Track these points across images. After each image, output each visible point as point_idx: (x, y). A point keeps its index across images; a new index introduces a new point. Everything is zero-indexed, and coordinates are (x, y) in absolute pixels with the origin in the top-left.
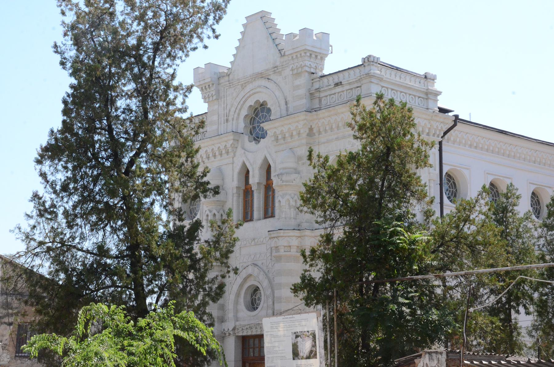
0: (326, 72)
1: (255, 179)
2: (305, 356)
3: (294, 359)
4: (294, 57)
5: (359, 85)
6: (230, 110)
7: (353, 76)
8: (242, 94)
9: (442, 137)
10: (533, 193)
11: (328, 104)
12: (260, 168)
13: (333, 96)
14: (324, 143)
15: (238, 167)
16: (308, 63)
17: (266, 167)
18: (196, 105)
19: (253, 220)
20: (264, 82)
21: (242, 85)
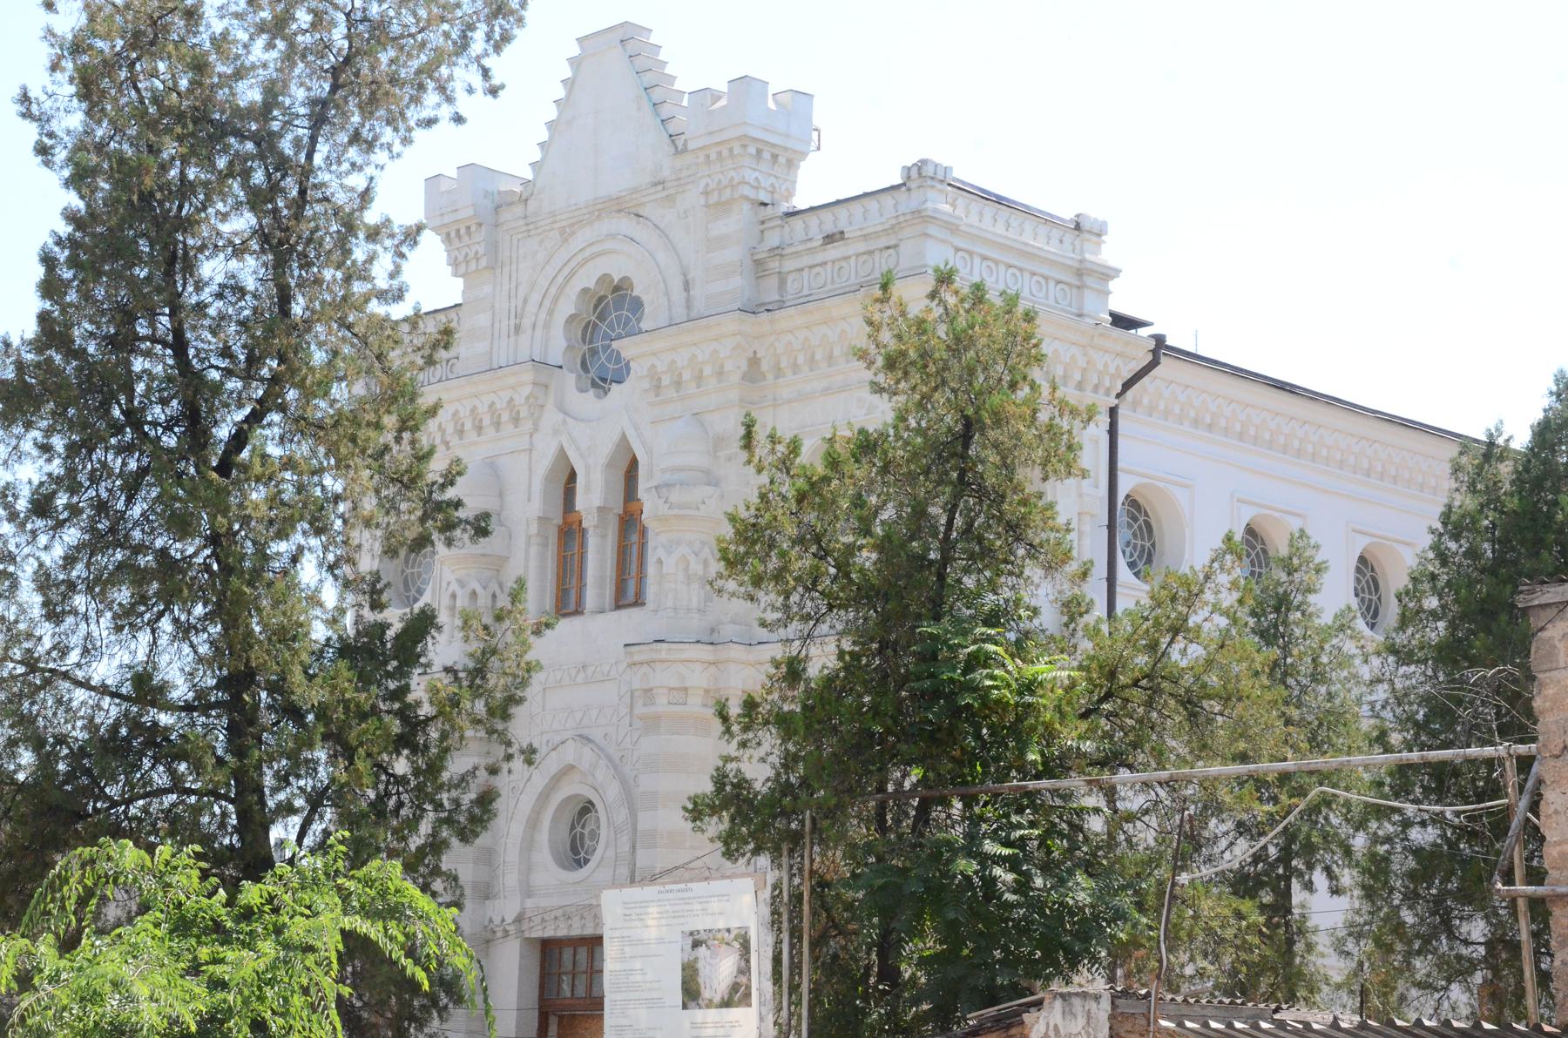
0: (801, 201)
1: (593, 496)
2: (717, 999)
4: (713, 157)
5: (892, 243)
6: (525, 301)
7: (878, 216)
9: (1118, 396)
10: (1362, 560)
11: (806, 292)
12: (610, 465)
13: (891, 251)
14: (789, 401)
15: (544, 461)
16: (750, 175)
17: (625, 465)
18: (430, 281)
19: (581, 613)
20: (625, 225)
21: (562, 231)
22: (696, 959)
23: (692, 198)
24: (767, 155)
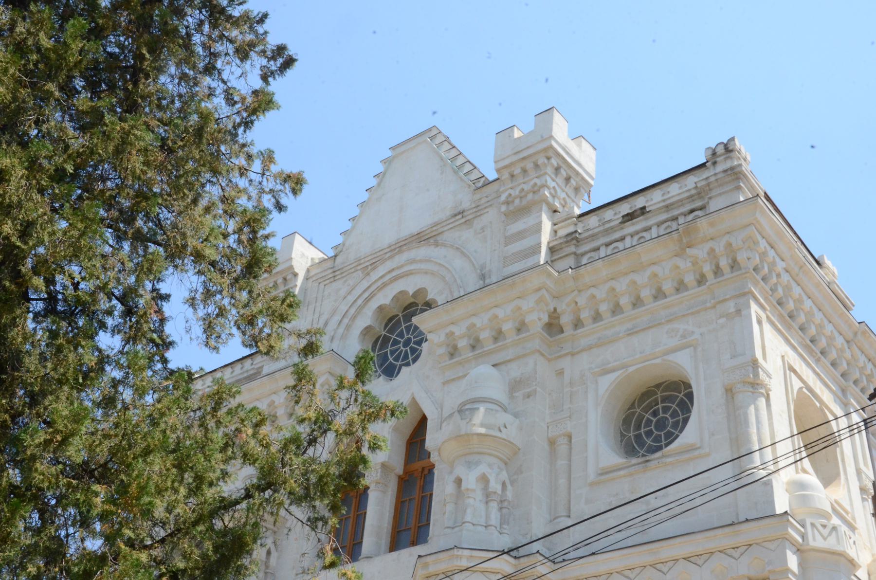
8: (365, 284)
14: (590, 348)
20: (423, 252)
23: (491, 216)
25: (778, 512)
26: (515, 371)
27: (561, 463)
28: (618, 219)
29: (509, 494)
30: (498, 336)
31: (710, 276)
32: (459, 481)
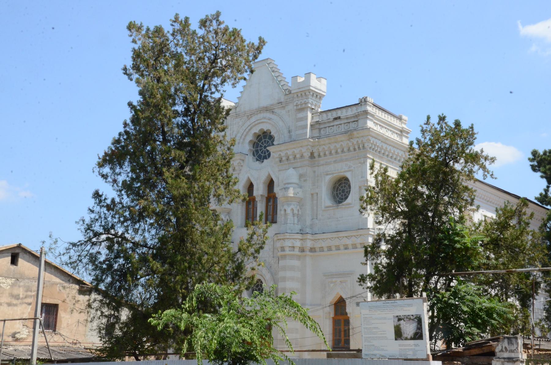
1: (259, 191)
2: (409, 337)
3: (396, 339)
4: (299, 95)
5: (356, 120)
7: (350, 112)
8: (248, 123)
11: (327, 134)
12: (264, 183)
14: (323, 165)
20: (268, 115)
21: (248, 116)
22: (400, 325)
23: (291, 107)
24: (315, 95)
25: (351, 348)
26: (301, 171)
27: (315, 202)
28: (332, 118)
29: (300, 213)
30: (295, 158)
31: (357, 149)
32: (285, 210)
